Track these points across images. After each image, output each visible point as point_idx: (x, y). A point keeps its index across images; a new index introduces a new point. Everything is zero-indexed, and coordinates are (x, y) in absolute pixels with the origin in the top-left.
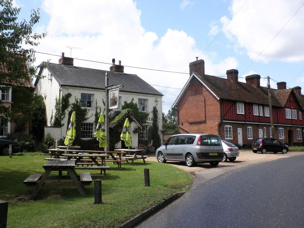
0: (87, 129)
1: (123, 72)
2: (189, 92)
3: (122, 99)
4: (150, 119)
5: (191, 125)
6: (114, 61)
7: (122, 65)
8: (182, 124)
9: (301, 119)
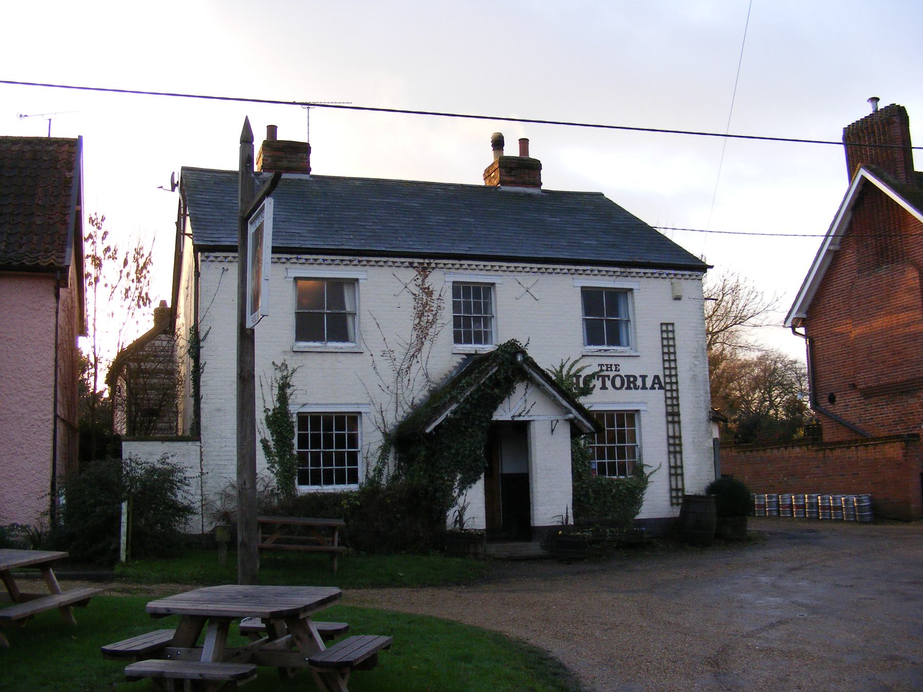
0: (340, 444)
1: (540, 184)
2: (850, 258)
3: (498, 293)
4: (649, 383)
5: (867, 402)
6: (498, 143)
7: (533, 155)
8: (832, 399)
9: (182, 236)
